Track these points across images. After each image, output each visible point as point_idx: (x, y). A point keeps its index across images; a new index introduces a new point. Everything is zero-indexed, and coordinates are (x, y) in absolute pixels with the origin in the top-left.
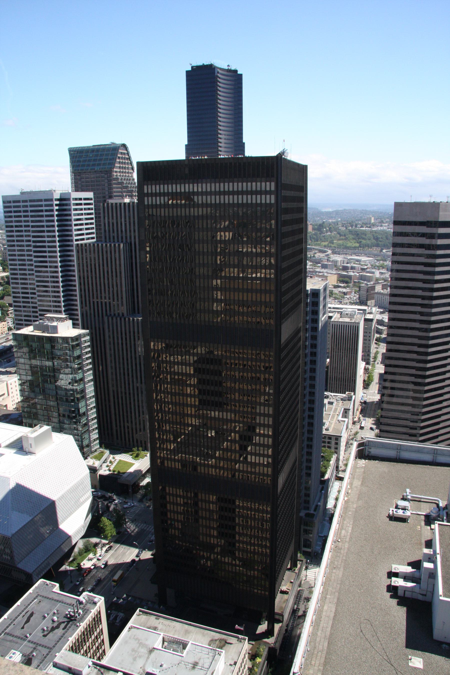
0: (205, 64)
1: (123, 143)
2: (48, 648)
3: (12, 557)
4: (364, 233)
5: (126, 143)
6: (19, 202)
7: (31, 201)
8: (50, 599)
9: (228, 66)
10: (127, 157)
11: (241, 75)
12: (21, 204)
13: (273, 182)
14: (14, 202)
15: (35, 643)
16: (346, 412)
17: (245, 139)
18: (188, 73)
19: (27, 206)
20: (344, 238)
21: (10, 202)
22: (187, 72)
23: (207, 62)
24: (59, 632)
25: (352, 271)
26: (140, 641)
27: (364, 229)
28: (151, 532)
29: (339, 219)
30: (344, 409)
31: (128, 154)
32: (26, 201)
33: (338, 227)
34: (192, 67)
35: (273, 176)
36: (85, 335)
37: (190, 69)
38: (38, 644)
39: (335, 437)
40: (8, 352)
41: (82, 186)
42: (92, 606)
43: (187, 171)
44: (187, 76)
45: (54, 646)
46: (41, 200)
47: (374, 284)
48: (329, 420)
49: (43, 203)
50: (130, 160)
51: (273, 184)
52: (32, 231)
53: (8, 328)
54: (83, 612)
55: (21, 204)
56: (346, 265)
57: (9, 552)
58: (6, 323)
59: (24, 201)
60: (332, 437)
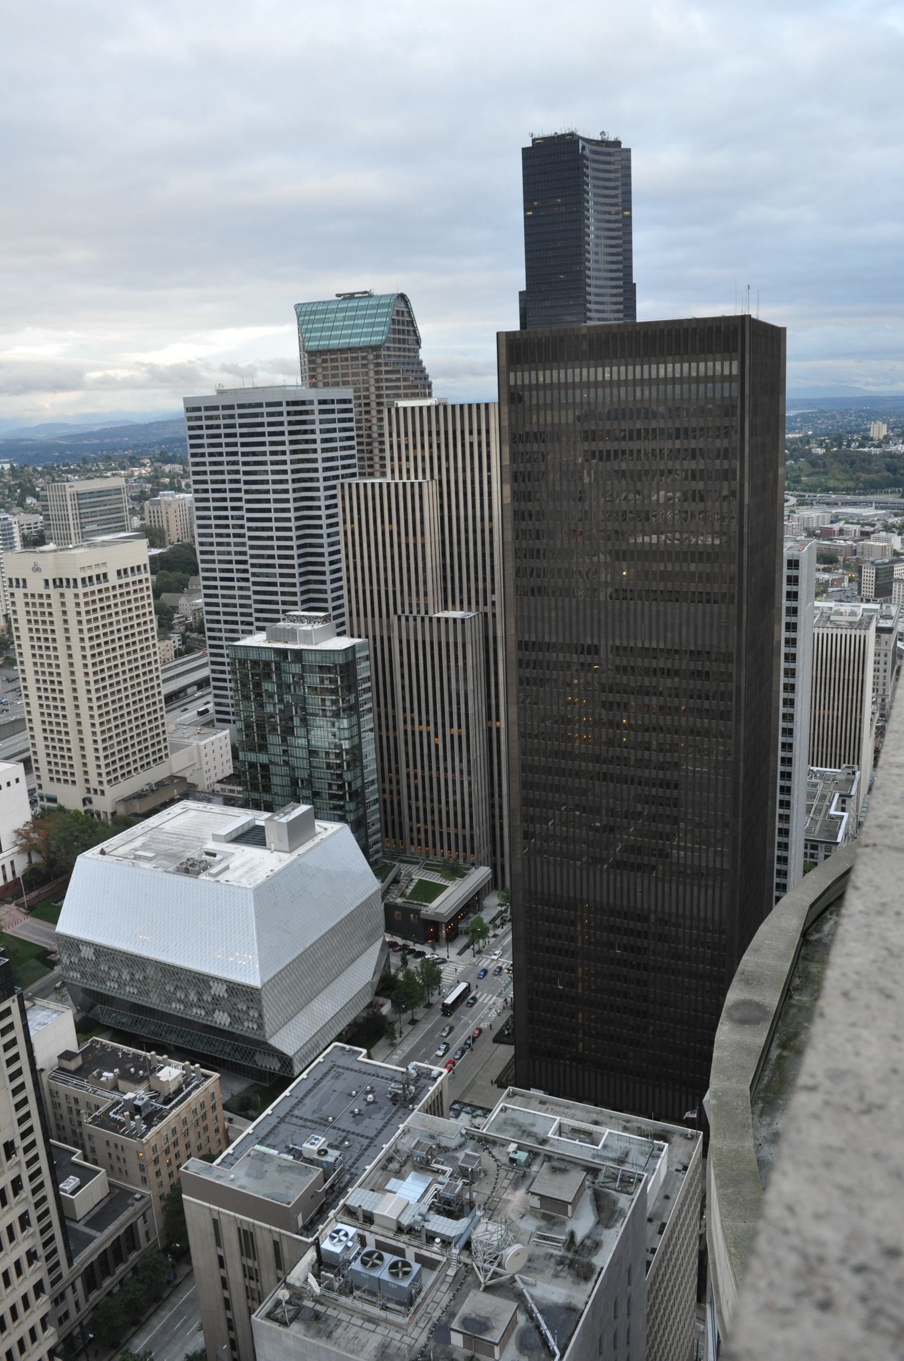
0: (559, 133)
1: (400, 292)
2: (367, 1137)
3: (261, 1027)
4: (868, 458)
5: (405, 293)
6: (216, 408)
7: (241, 406)
8: (356, 1071)
9: (603, 133)
10: (409, 319)
11: (628, 151)
12: (221, 412)
13: (736, 359)
14: (207, 409)
15: (344, 1131)
16: (844, 802)
17: (637, 277)
18: (527, 153)
19: (232, 417)
20: (822, 470)
21: (198, 409)
22: (525, 150)
23: (560, 128)
24: (377, 1121)
25: (841, 537)
26: (523, 1128)
27: (866, 450)
28: (486, 1004)
29: (810, 433)
30: (840, 796)
31: (410, 313)
32: (231, 407)
33: (810, 449)
34: (534, 140)
35: (735, 350)
36: (362, 647)
37: (530, 145)
38: (348, 1132)
39: (824, 845)
40: (182, 695)
41: (325, 376)
42: (430, 1082)
43: (585, 346)
44: (525, 159)
45: (376, 1136)
46: (260, 405)
47: (890, 562)
48: (811, 815)
49: (265, 410)
50: (413, 325)
51: (735, 365)
52: (238, 464)
53: (175, 652)
54: (416, 1089)
55: (221, 412)
56: (830, 526)
57: (256, 1015)
58: (171, 641)
59: (225, 408)
60: (820, 845)
